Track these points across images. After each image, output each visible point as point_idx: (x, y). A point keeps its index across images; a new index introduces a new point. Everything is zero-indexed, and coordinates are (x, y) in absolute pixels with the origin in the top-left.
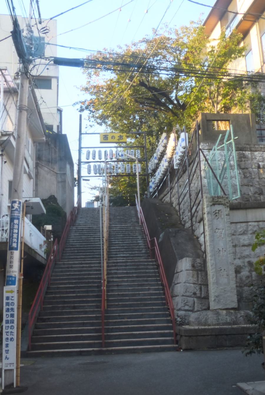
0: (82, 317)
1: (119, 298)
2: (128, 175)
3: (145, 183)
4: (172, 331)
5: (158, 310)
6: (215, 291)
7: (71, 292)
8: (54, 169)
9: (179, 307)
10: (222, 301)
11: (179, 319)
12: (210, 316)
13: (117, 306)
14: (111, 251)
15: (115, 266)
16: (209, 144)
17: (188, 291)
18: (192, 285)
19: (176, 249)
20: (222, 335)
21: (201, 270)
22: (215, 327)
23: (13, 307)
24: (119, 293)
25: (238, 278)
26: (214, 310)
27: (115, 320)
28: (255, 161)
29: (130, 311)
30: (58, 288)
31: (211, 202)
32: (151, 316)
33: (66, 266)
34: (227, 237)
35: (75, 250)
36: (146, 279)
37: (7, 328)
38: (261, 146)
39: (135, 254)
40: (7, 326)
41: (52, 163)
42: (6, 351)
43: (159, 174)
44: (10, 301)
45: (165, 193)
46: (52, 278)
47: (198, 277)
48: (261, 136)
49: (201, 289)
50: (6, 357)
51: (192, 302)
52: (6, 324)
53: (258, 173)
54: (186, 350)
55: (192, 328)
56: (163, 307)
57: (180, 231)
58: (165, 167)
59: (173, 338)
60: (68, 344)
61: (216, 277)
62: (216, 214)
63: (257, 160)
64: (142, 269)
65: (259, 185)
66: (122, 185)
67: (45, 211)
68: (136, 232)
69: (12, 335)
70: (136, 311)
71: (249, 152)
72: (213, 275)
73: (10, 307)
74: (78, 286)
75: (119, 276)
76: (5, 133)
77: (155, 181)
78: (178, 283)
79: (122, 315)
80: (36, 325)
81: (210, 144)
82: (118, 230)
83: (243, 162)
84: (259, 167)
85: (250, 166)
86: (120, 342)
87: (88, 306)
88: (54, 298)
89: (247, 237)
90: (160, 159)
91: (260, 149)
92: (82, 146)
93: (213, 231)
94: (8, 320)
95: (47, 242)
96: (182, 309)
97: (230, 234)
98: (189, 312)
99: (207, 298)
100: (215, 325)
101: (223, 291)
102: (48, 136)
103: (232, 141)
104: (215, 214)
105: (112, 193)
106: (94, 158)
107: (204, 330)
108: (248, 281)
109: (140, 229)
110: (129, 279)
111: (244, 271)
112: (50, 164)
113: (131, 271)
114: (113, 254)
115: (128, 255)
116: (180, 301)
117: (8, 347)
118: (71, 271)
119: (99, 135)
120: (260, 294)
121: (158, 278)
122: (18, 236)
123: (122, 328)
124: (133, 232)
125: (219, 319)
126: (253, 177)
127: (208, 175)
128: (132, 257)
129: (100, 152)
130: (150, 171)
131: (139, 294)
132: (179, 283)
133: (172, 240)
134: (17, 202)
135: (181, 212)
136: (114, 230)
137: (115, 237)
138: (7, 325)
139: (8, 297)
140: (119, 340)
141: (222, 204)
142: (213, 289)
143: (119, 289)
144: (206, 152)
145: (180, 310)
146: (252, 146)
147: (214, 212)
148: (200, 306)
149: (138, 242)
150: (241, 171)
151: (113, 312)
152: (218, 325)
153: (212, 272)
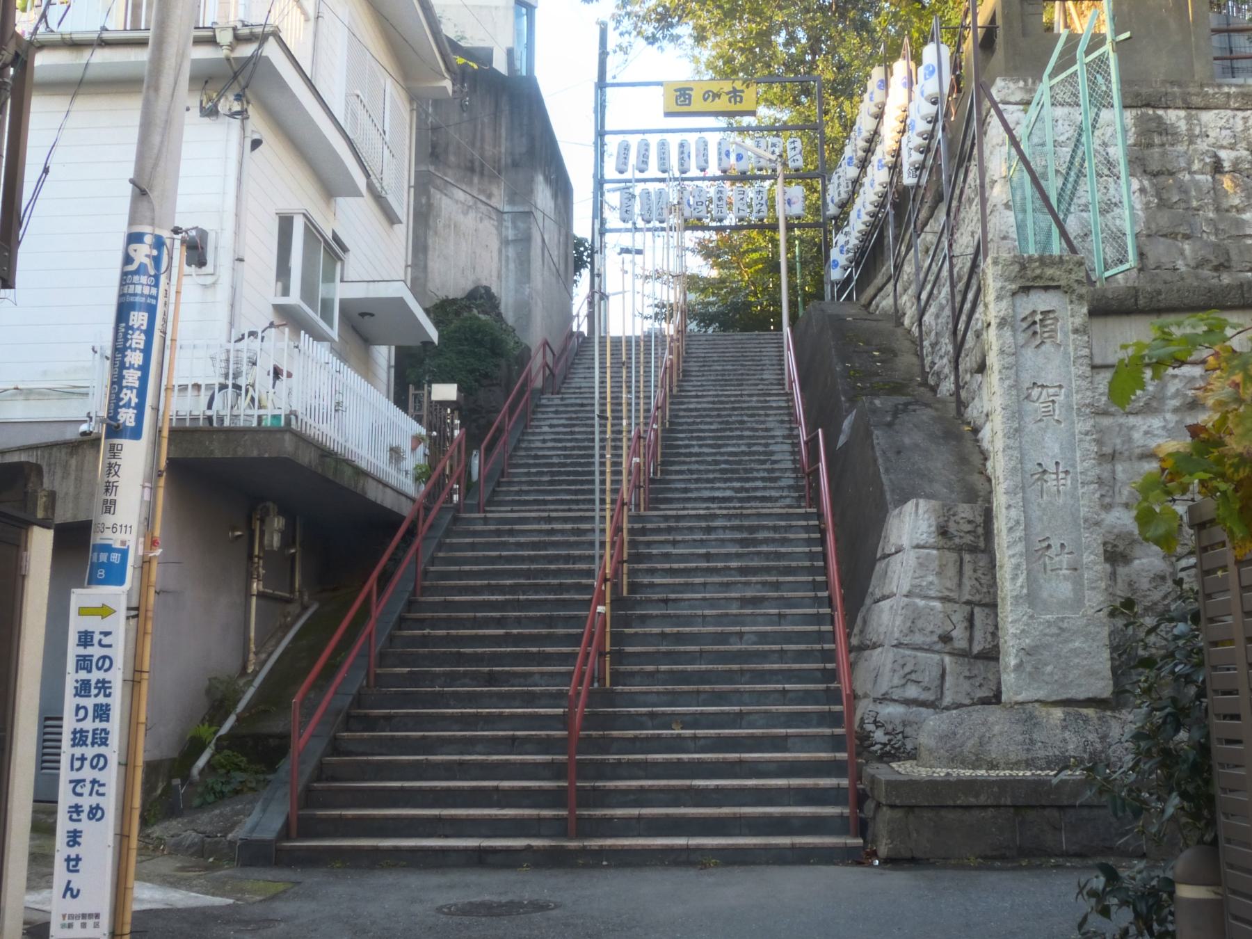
0: (512, 716)
1: (663, 648)
2: (761, 227)
3: (819, 254)
4: (845, 782)
5: (806, 697)
6: (1023, 631)
7: (487, 623)
8: (490, 196)
9: (883, 687)
10: (1049, 669)
11: (879, 736)
12: (997, 729)
13: (651, 677)
14: (668, 477)
15: (669, 530)
16: (1026, 84)
17: (921, 630)
18: (937, 604)
19: (887, 470)
20: (1044, 807)
21: (973, 549)
22: (1014, 773)
23: (107, 676)
24: (668, 630)
25: (1119, 581)
26: (1017, 703)
27: (631, 733)
28: (1202, 145)
29: (696, 698)
30: (448, 605)
31: (1013, 280)
32: (773, 720)
33: (492, 527)
34: (1076, 419)
35: (542, 474)
36: (774, 579)
37: (77, 764)
38: (1226, 89)
39: (756, 489)
40: (78, 755)
41: (482, 174)
42: (68, 859)
43: (859, 216)
44: (95, 651)
45: (879, 281)
46: (432, 569)
47: (960, 572)
48: (1228, 55)
49: (970, 620)
50: (68, 888)
51: (936, 672)
52: (73, 746)
53: (1214, 189)
54: (892, 862)
55: (923, 773)
56: (822, 686)
57: (911, 407)
58: (879, 189)
59: (846, 811)
60: (439, 819)
61: (1028, 578)
62: (1035, 328)
63: (1211, 140)
64: (766, 541)
65: (1216, 235)
66: (748, 266)
67: (434, 334)
68: (767, 415)
69: (98, 794)
70: (719, 698)
71: (1182, 113)
72: (1017, 566)
73: (95, 676)
74: (518, 600)
75: (675, 566)
76: (246, 31)
77: (847, 242)
78: (884, 598)
79: (664, 714)
80: (335, 738)
81: (1030, 81)
82: (705, 409)
83: (1157, 150)
84: (1217, 168)
85: (1183, 165)
86: (639, 818)
87: (542, 674)
88: (425, 641)
89: (1162, 424)
90: (864, 164)
91: (1223, 99)
92: (608, 128)
93: (1021, 394)
94: (82, 731)
95: (437, 446)
96: (895, 697)
97: (1087, 405)
98: (923, 710)
99: (991, 655)
100: (1016, 765)
101: (1054, 630)
102: (460, 76)
103: (1108, 48)
104: (1029, 327)
105: (713, 294)
106: (643, 166)
107: (970, 785)
108: (1162, 594)
109: (784, 404)
110: (709, 580)
111: (1148, 555)
112: (476, 180)
113: (723, 551)
114: (677, 489)
115: (728, 493)
116: (889, 666)
117: (79, 844)
118: (504, 545)
119: (660, 89)
120: (1171, 655)
121: (819, 578)
122: (144, 380)
123: (655, 764)
124: (759, 415)
125: (1032, 742)
126: (1195, 204)
127: (1018, 198)
128: (741, 500)
129: (663, 145)
130: (832, 210)
131: (741, 635)
132: (888, 597)
133: (880, 438)
134: (148, 239)
135: (926, 343)
136: (692, 406)
137: (692, 431)
138: (78, 751)
139: (86, 632)
140: (635, 812)
141: (1058, 287)
142: (1013, 622)
143: (669, 616)
144: (1013, 114)
145: (884, 699)
146: (1193, 89)
147: (1024, 319)
148: (966, 686)
149: (772, 448)
150: (1146, 183)
151: (632, 699)
152: (1029, 764)
153: (1013, 556)
